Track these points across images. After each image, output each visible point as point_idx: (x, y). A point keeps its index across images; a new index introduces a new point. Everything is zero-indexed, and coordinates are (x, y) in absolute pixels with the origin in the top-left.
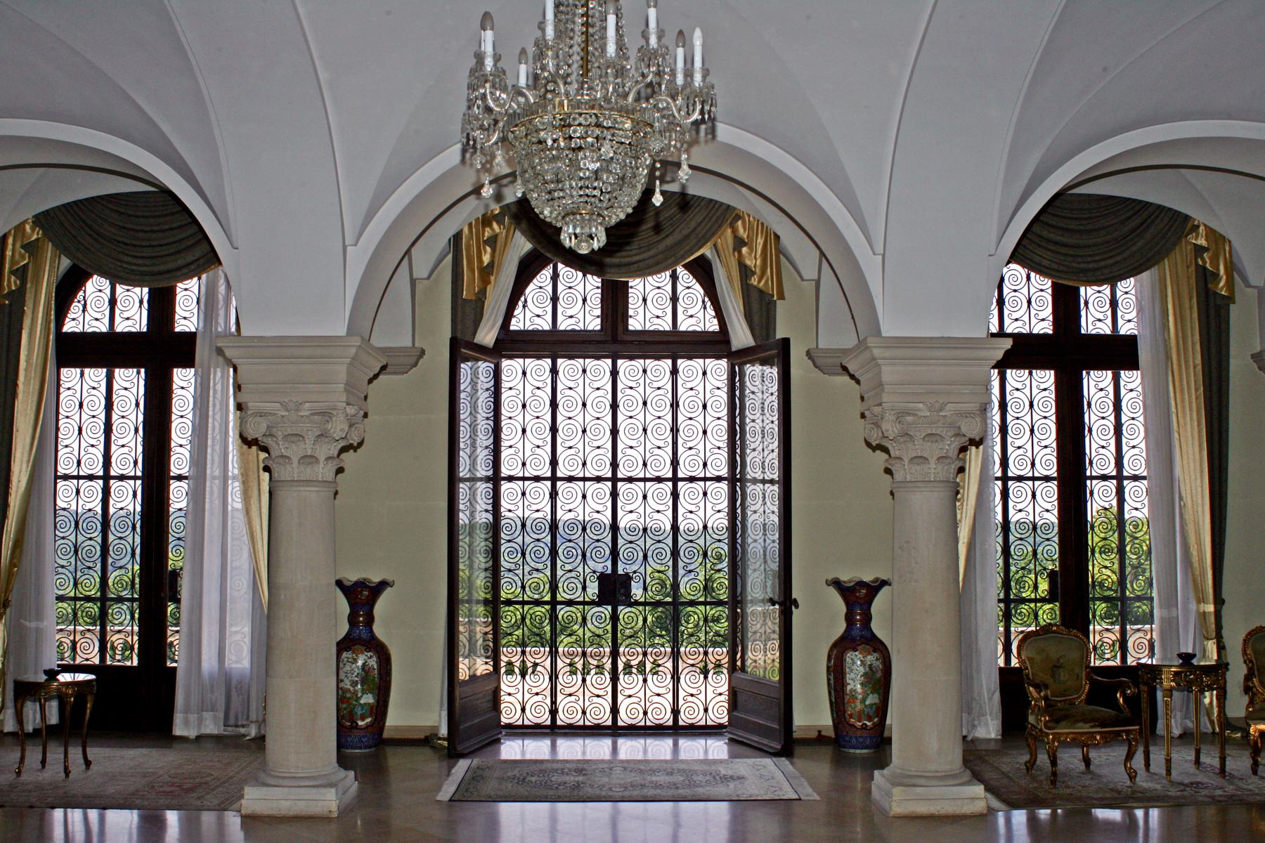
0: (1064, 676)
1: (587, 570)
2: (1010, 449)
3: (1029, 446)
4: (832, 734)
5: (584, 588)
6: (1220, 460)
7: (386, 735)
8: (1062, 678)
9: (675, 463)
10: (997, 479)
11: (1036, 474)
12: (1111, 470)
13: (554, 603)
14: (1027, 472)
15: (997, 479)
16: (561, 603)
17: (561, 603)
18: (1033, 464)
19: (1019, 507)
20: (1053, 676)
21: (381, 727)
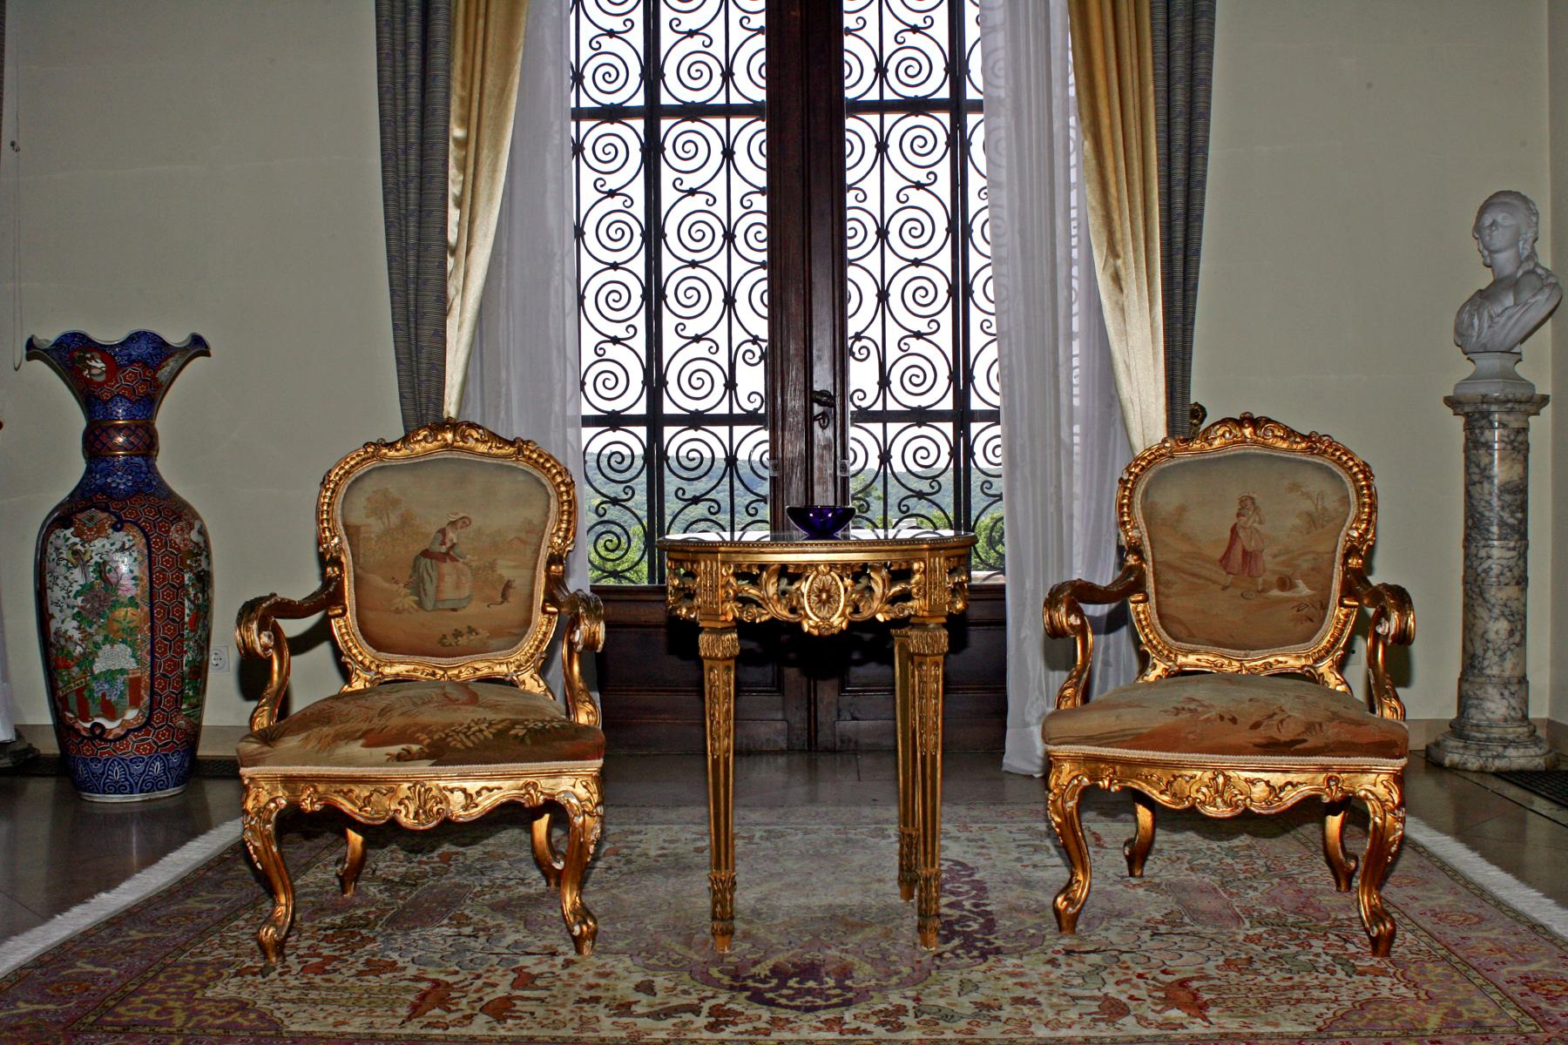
0: (451, 582)
1: (739, 336)
2: (667, 38)
3: (717, 30)
4: (49, 746)
5: (731, 385)
6: (1192, 57)
7: (203, 751)
8: (449, 592)
9: (652, 73)
10: (977, 106)
11: (736, 99)
12: (936, 85)
13: (655, 420)
14: (711, 93)
15: (977, 106)
16: (636, 420)
17: (636, 420)
18: (728, 74)
19: (691, 182)
20: (417, 587)
21: (192, 735)
